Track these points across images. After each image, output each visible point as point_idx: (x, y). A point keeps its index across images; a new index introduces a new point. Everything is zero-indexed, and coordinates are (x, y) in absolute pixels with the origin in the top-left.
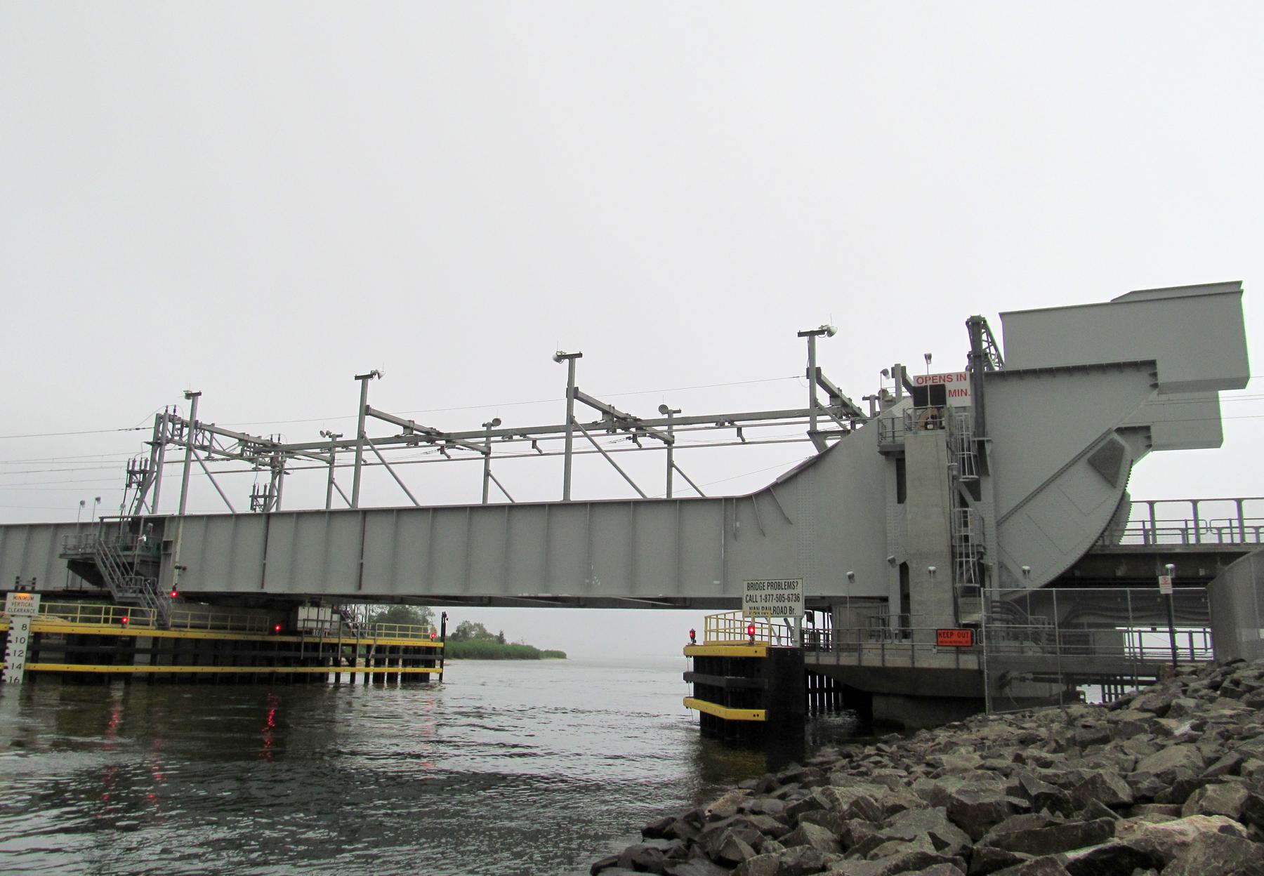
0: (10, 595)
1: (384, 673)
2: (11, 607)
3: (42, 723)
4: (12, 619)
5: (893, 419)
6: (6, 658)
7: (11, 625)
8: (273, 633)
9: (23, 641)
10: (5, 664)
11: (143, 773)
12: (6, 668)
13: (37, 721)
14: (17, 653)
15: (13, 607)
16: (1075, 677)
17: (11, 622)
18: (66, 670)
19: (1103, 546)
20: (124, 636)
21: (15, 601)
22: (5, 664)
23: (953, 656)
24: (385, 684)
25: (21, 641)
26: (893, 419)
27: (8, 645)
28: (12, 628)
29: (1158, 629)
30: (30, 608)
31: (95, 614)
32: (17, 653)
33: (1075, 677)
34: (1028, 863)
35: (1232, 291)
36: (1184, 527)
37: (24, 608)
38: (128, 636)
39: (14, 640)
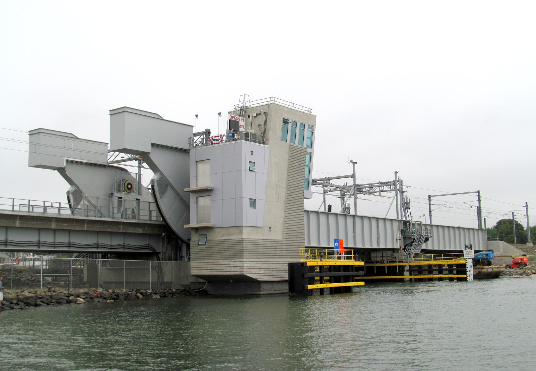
1: (385, 266)
3: (58, 367)
4: (466, 259)
5: (14, 199)
6: (467, 273)
7: (467, 262)
8: (9, 262)
12: (468, 276)
13: (59, 367)
14: (470, 271)
15: (466, 255)
18: (438, 277)
20: (326, 266)
23: (41, 240)
24: (41, 288)
25: (471, 267)
26: (14, 199)
27: (467, 268)
28: (467, 263)
30: (471, 255)
31: (105, 260)
32: (470, 271)
36: (59, 206)
38: (328, 266)
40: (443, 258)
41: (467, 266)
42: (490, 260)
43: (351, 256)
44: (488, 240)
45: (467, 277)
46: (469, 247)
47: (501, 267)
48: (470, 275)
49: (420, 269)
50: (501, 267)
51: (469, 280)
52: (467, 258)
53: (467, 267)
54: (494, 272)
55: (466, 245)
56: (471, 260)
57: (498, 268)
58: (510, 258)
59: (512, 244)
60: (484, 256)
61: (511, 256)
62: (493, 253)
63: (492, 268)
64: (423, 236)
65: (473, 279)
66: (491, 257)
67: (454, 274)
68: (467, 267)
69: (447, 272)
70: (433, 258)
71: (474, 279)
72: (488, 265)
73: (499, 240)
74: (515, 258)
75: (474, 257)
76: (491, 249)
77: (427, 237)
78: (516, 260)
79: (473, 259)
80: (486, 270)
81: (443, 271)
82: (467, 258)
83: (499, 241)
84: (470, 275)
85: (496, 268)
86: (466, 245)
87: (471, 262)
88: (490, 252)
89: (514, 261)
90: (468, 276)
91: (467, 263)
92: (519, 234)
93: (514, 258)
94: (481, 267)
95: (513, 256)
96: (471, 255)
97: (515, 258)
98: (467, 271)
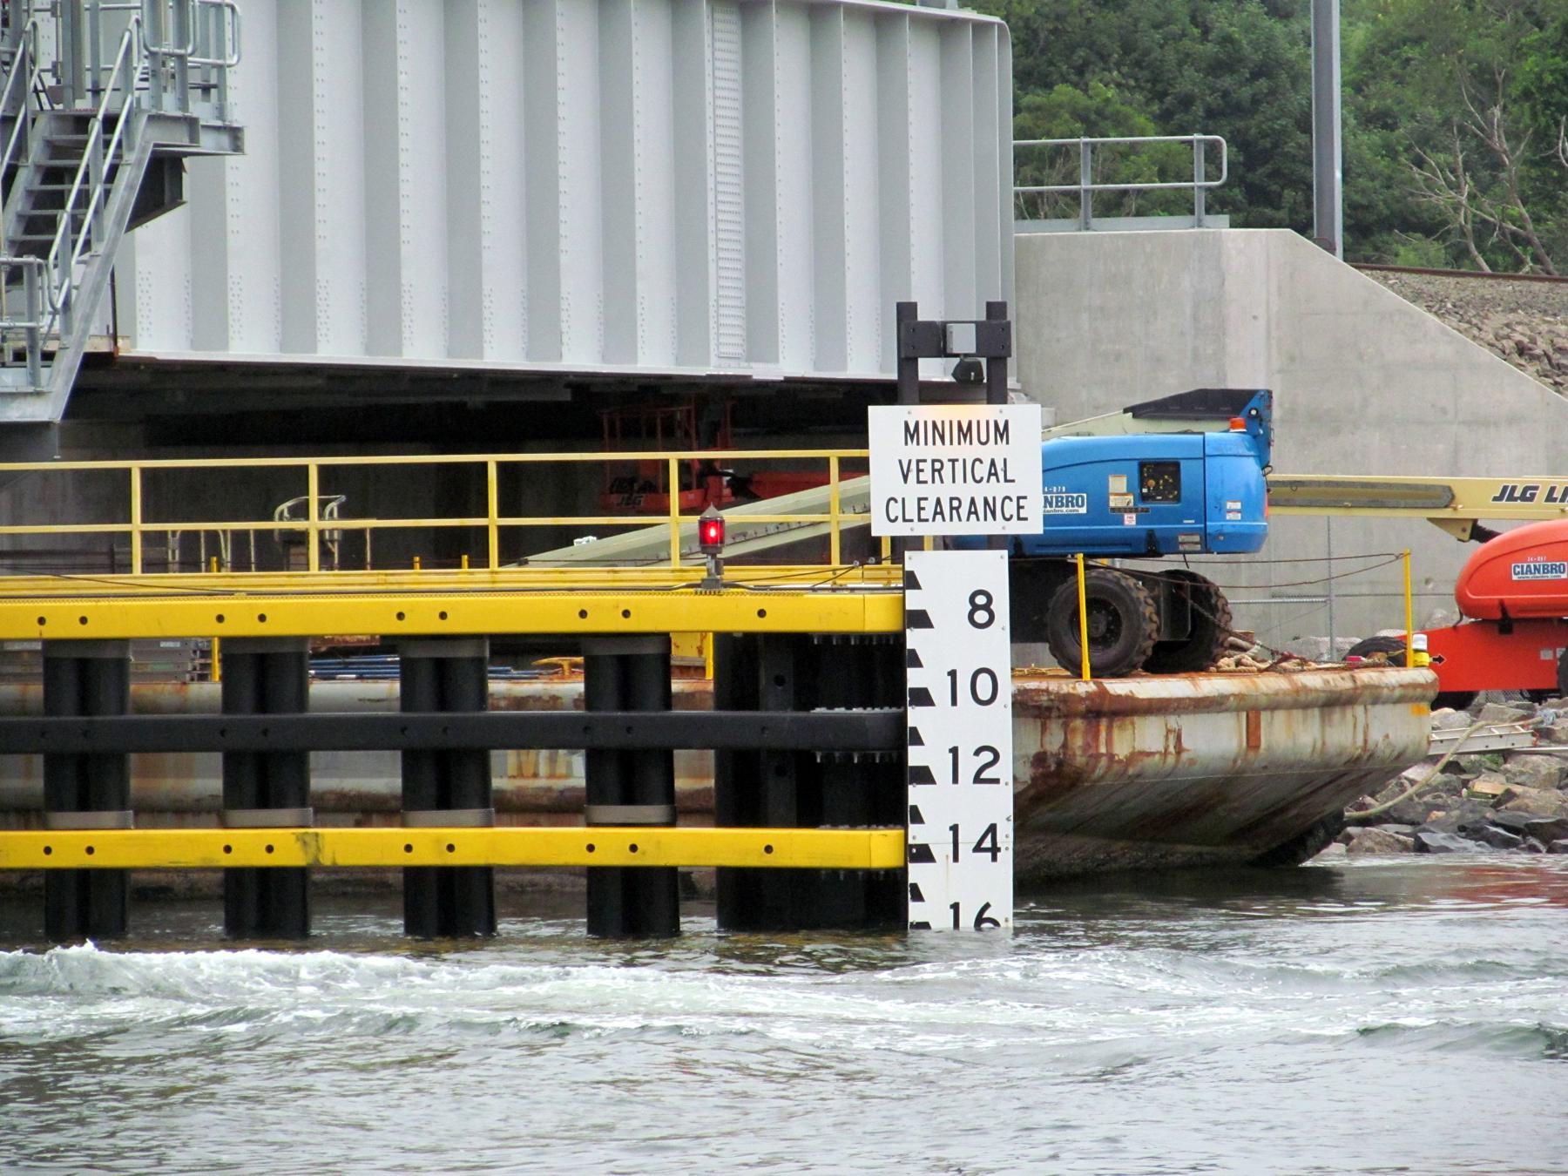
0: (883, 420)
2: (898, 489)
4: (913, 560)
6: (916, 795)
7: (914, 600)
9: (984, 691)
10: (917, 835)
11: (777, 956)
12: (923, 854)
14: (968, 766)
15: (912, 491)
16: (163, 645)
17: (911, 581)
19: (1249, 450)
21: (914, 451)
22: (917, 835)
27: (916, 716)
28: (920, 619)
29: (178, 645)
30: (995, 490)
32: (968, 766)
33: (163, 645)
34: (1371, 811)
35: (899, 305)
37: (966, 491)
39: (940, 691)
40: (493, 521)
41: (914, 678)
42: (1209, 567)
43: (128, 535)
44: (1029, 208)
45: (917, 873)
46: (964, 341)
47: (1375, 696)
48: (968, 839)
49: (85, 704)
50: (1375, 696)
51: (941, 919)
52: (916, 543)
53: (923, 698)
54: (1279, 770)
55: (906, 311)
56: (993, 571)
57: (1333, 703)
58: (1416, 520)
59: (1447, 286)
60: (1119, 491)
61: (1446, 497)
62: (1261, 445)
63: (1252, 711)
64: (110, 123)
65: (1003, 907)
66: (1233, 515)
67: (679, 812)
68: (923, 698)
69: (28, 774)
70: (137, 526)
71: (1026, 886)
72: (1163, 661)
73: (1217, 203)
74: (1507, 533)
75: (1034, 526)
76: (1238, 380)
77: (176, 139)
78: (1519, 572)
79: (1017, 548)
80: (1148, 736)
81: (316, 758)
82: (916, 543)
83: (1220, 227)
84: (968, 839)
85: (1300, 703)
86: (906, 311)
87: (979, 604)
88: (1216, 434)
89: (1474, 574)
90: (923, 854)
91: (920, 619)
92: (1217, 67)
93: (1480, 534)
94: (1085, 687)
95: (1476, 504)
96: (995, 490)
97: (1509, 522)
98: (915, 757)
